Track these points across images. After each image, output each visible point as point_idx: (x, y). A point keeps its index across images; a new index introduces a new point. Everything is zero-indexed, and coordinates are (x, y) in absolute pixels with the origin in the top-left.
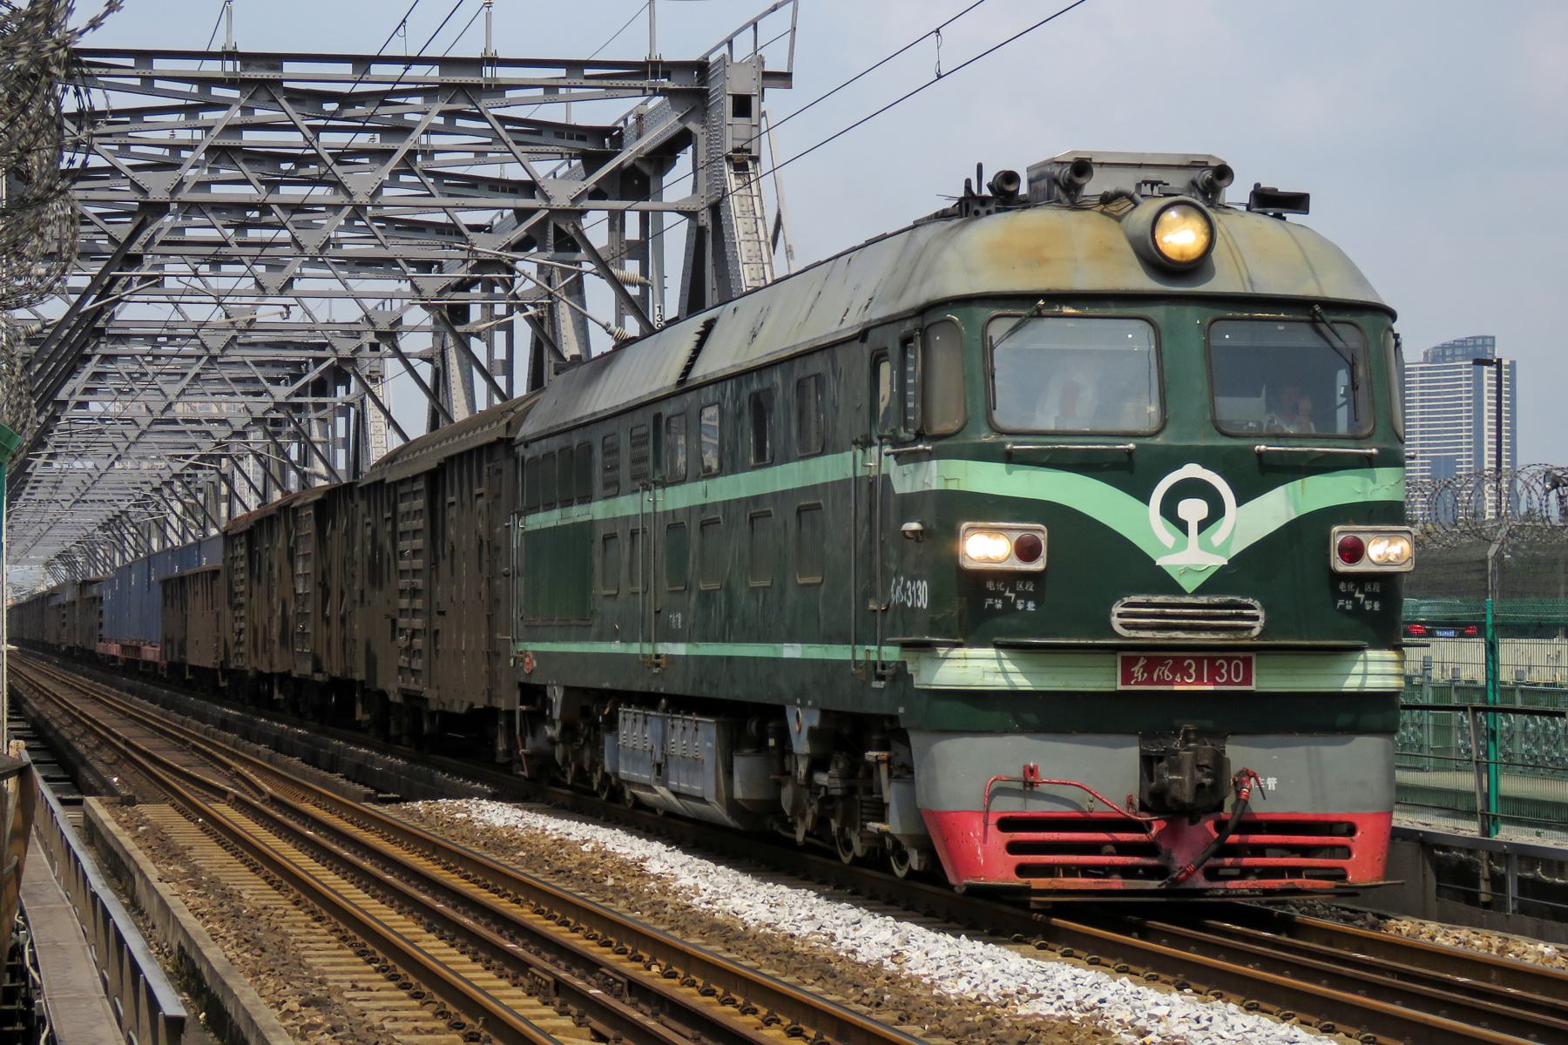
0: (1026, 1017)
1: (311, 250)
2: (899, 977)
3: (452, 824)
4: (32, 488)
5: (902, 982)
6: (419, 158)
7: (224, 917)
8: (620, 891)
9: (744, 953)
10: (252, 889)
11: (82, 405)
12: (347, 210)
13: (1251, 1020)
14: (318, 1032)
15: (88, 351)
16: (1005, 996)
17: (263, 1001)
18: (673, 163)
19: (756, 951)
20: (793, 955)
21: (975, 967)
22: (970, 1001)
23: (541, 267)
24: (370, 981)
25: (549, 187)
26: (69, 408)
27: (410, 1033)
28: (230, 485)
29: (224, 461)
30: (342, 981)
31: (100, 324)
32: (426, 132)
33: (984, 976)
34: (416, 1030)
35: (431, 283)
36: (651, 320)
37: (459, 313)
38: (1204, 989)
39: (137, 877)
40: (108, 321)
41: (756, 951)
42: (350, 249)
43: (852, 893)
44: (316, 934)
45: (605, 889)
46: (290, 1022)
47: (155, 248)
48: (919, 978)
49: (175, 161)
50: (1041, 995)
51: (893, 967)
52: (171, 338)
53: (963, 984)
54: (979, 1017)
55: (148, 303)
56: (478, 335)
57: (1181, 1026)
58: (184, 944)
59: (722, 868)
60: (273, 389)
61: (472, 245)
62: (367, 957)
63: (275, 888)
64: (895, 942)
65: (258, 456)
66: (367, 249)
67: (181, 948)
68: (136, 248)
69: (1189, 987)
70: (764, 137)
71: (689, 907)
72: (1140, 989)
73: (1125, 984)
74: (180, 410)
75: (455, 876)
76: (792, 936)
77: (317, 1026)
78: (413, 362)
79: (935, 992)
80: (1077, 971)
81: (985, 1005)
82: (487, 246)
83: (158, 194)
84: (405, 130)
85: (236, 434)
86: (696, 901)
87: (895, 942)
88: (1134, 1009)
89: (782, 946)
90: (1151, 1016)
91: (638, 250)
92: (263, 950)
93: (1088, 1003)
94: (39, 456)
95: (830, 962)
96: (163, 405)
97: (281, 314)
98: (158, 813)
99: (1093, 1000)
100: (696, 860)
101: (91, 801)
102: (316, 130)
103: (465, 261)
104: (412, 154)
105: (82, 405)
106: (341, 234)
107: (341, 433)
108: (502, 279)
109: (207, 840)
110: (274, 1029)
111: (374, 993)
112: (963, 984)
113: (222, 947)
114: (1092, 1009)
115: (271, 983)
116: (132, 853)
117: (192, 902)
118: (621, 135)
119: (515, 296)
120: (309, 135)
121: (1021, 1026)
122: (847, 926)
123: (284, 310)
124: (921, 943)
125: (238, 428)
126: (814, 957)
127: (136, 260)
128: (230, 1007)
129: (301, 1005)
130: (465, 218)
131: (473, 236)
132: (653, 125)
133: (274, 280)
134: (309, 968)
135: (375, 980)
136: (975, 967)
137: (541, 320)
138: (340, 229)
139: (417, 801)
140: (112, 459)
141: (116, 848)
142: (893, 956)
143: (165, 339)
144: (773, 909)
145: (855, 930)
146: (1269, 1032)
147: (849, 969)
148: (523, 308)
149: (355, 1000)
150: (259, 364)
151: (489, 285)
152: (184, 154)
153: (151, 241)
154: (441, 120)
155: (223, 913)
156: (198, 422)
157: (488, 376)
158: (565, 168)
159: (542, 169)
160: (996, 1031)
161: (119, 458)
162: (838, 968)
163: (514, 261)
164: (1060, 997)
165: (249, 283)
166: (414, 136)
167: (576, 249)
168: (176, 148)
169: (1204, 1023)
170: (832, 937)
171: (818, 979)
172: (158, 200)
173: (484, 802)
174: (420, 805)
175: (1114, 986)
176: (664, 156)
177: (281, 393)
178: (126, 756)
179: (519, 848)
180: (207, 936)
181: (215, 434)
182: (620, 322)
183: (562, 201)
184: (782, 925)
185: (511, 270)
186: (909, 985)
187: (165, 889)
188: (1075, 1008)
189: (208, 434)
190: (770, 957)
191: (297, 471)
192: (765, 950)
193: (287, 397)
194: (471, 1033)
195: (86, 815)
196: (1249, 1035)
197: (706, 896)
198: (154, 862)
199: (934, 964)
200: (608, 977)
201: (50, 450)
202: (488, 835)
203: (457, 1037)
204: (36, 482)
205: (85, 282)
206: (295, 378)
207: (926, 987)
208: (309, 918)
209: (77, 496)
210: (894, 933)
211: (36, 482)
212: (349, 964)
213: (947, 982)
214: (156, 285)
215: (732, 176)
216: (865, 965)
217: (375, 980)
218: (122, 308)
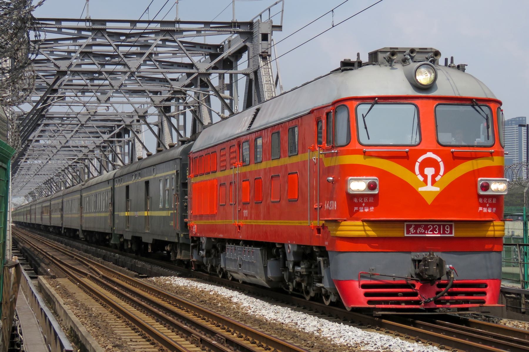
1: (116, 87)
2: (320, 337)
3: (165, 285)
4: (20, 170)
5: (321, 339)
6: (153, 55)
7: (86, 317)
8: (223, 308)
9: (266, 329)
10: (96, 307)
11: (37, 141)
12: (129, 73)
15: (39, 122)
16: (356, 344)
17: (100, 345)
18: (241, 57)
19: (270, 329)
20: (283, 330)
21: (346, 334)
22: (344, 346)
24: (137, 338)
25: (198, 65)
28: (88, 169)
29: (86, 160)
30: (127, 339)
31: (43, 113)
32: (156, 47)
33: (349, 337)
35: (158, 99)
36: (233, 111)
37: (167, 109)
38: (426, 341)
39: (56, 303)
41: (270, 329)
42: (130, 87)
44: (118, 322)
45: (218, 307)
47: (62, 87)
48: (326, 338)
50: (369, 344)
51: (318, 334)
52: (68, 118)
53: (342, 340)
55: (60, 106)
58: (72, 326)
59: (258, 300)
60: (103, 135)
61: (172, 85)
62: (136, 331)
63: (104, 307)
64: (318, 325)
65: (98, 159)
66: (135, 87)
67: (71, 328)
68: (56, 87)
69: (420, 341)
70: (272, 48)
71: (247, 313)
72: (403, 341)
73: (398, 340)
74: (71, 143)
75: (166, 303)
76: (283, 323)
78: (151, 126)
79: (332, 342)
80: (381, 335)
81: (349, 347)
82: (177, 86)
83: (63, 68)
84: (148, 46)
85: (90, 151)
86: (249, 311)
87: (318, 325)
91: (230, 87)
92: (100, 328)
93: (385, 346)
94: (23, 159)
95: (296, 332)
96: (65, 141)
97: (106, 109)
98: (64, 281)
99: (387, 345)
100: (249, 297)
101: (41, 277)
102: (118, 46)
103: (169, 91)
104: (151, 54)
105: (37, 141)
108: (182, 97)
109: (80, 290)
111: (138, 343)
112: (342, 340)
113: (85, 327)
114: (387, 348)
115: (102, 339)
116: (54, 295)
117: (75, 311)
118: (223, 47)
119: (187, 103)
120: (115, 48)
122: (302, 320)
123: (107, 108)
124: (327, 326)
125: (91, 149)
127: (56, 91)
128: (88, 347)
130: (169, 76)
131: (172, 82)
133: (104, 98)
134: (116, 334)
135: (138, 338)
136: (346, 334)
137: (196, 111)
138: (126, 80)
139: (153, 277)
140: (48, 160)
142: (317, 330)
143: (66, 118)
144: (276, 314)
145: (304, 321)
147: (302, 335)
148: (189, 107)
149: (131, 345)
150: (98, 127)
151: (178, 99)
152: (73, 54)
153: (61, 84)
154: (161, 42)
155: (86, 315)
156: (77, 147)
159: (196, 59)
161: (50, 159)
162: (299, 334)
163: (186, 91)
164: (376, 344)
165: (94, 99)
166: (152, 48)
167: (208, 87)
168: (69, 52)
170: (296, 324)
171: (292, 338)
172: (63, 70)
173: (176, 277)
174: (154, 279)
175: (394, 340)
176: (238, 54)
177: (106, 137)
179: (188, 293)
180: (80, 323)
182: (223, 112)
183: (203, 70)
184: (279, 320)
185: (185, 94)
186: (323, 340)
187: (66, 307)
188: (381, 348)
190: (275, 330)
191: (112, 164)
192: (273, 328)
193: (108, 138)
195: (39, 282)
197: (253, 310)
198: (62, 298)
199: (332, 333)
201: (26, 156)
202: (177, 289)
204: (22, 168)
205: (38, 99)
206: (111, 132)
207: (329, 341)
208: (115, 317)
209: (36, 173)
210: (318, 322)
211: (22, 168)
212: (129, 333)
213: (336, 339)
214: (62, 100)
215: (262, 61)
216: (308, 333)
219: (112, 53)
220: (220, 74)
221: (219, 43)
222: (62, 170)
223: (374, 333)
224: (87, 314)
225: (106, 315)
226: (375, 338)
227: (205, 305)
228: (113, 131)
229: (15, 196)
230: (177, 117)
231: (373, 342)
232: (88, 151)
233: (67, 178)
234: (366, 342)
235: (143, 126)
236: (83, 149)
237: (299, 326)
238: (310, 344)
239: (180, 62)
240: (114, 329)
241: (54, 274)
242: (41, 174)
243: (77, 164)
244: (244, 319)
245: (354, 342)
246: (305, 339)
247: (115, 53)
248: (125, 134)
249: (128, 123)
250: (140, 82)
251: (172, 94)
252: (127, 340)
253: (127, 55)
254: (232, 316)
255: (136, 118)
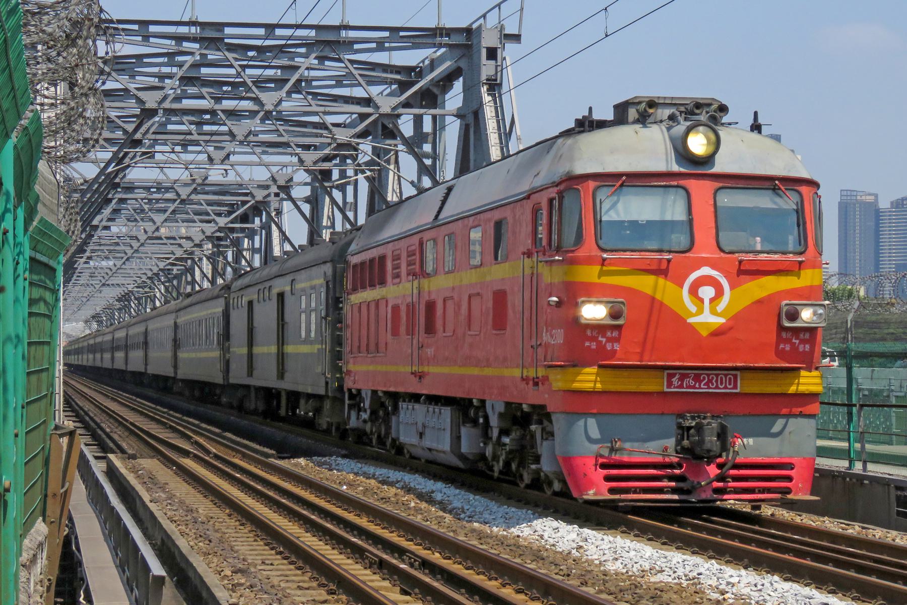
0: (655, 583)
1: (240, 137)
4: (78, 276)
6: (303, 84)
9: (490, 545)
10: (204, 507)
11: (107, 228)
12: (262, 114)
13: (787, 585)
14: (243, 588)
15: (110, 196)
16: (643, 571)
18: (451, 87)
19: (497, 545)
20: (519, 547)
21: (625, 554)
23: (374, 148)
25: (379, 101)
26: (99, 229)
27: (296, 589)
28: (193, 276)
29: (189, 262)
30: (257, 560)
31: (117, 180)
32: (307, 69)
34: (300, 588)
36: (438, 178)
37: (327, 174)
39: (137, 500)
40: (122, 179)
41: (497, 545)
42: (263, 137)
43: (554, 512)
45: (409, 508)
46: (226, 582)
47: (149, 136)
48: (593, 561)
49: (160, 84)
50: (664, 571)
51: (578, 554)
54: (628, 583)
55: (145, 167)
56: (337, 187)
57: (746, 588)
59: (477, 497)
60: (218, 219)
62: (271, 546)
65: (208, 258)
67: (163, 540)
68: (138, 136)
70: (504, 71)
72: (722, 567)
73: (714, 565)
75: (322, 500)
76: (518, 536)
77: (242, 585)
78: (299, 203)
79: (602, 568)
80: (685, 557)
81: (631, 576)
82: (343, 136)
83: (151, 104)
84: (297, 68)
85: (196, 245)
87: (578, 539)
88: (718, 579)
89: (512, 541)
90: (728, 583)
92: (210, 541)
93: (691, 575)
94: (82, 257)
95: (540, 551)
96: (154, 228)
98: (150, 464)
99: (695, 574)
100: (463, 492)
101: (111, 456)
102: (244, 67)
104: (299, 81)
106: (258, 129)
107: (257, 245)
110: (217, 586)
113: (187, 539)
115: (215, 560)
117: (169, 513)
118: (421, 71)
120: (239, 70)
121: (652, 588)
123: (224, 172)
124: (594, 541)
125: (197, 242)
126: (531, 548)
127: (138, 143)
128: (191, 574)
129: (232, 572)
130: (330, 119)
131: (334, 129)
132: (439, 66)
133: (218, 155)
137: (374, 178)
139: (300, 458)
140: (124, 260)
141: (125, 483)
143: (155, 190)
146: (797, 593)
148: (363, 172)
150: (210, 203)
151: (344, 158)
152: (167, 81)
153: (147, 132)
154: (316, 62)
155: (187, 521)
156: (174, 238)
157: (342, 211)
158: (388, 90)
159: (374, 91)
160: (638, 591)
163: (358, 144)
164: (675, 572)
166: (300, 71)
168: (162, 77)
169: (759, 587)
170: (542, 537)
172: (151, 107)
173: (339, 459)
175: (707, 565)
176: (447, 81)
177: (222, 221)
178: (133, 432)
180: (178, 533)
181: (184, 245)
183: (386, 109)
185: (356, 150)
186: (586, 564)
187: (153, 507)
188: (684, 578)
189: (180, 245)
190: (506, 547)
192: (502, 543)
194: (331, 590)
196: (785, 594)
199: (601, 552)
200: (410, 558)
201: (88, 254)
203: (323, 592)
204: (80, 273)
205: (109, 155)
206: (230, 213)
207: (596, 566)
208: (237, 523)
209: (103, 281)
210: (578, 535)
213: (609, 563)
215: (486, 94)
216: (561, 553)
217: (276, 559)
218: (130, 171)
219: (232, 80)
220: (415, 115)
221: (414, 64)
222: (149, 278)
223: (671, 553)
224: (189, 517)
225: (221, 520)
226: (674, 561)
227: (388, 504)
228: (234, 212)
229: (67, 320)
230: (342, 188)
231: (671, 568)
232: (193, 245)
233: (157, 290)
234: (657, 568)
235: (285, 203)
236: (183, 241)
237: (546, 541)
238: (565, 572)
239: (348, 94)
240: (234, 544)
241: (134, 452)
242: (112, 285)
243: (174, 267)
244: (454, 528)
245: (639, 568)
246: (557, 562)
247: (237, 80)
248: (255, 216)
249: (259, 198)
250: (281, 128)
251: (335, 149)
252: (256, 562)
253: (259, 83)
254: (433, 523)
255: (274, 189)
